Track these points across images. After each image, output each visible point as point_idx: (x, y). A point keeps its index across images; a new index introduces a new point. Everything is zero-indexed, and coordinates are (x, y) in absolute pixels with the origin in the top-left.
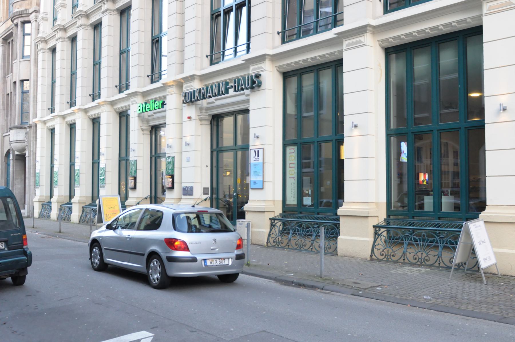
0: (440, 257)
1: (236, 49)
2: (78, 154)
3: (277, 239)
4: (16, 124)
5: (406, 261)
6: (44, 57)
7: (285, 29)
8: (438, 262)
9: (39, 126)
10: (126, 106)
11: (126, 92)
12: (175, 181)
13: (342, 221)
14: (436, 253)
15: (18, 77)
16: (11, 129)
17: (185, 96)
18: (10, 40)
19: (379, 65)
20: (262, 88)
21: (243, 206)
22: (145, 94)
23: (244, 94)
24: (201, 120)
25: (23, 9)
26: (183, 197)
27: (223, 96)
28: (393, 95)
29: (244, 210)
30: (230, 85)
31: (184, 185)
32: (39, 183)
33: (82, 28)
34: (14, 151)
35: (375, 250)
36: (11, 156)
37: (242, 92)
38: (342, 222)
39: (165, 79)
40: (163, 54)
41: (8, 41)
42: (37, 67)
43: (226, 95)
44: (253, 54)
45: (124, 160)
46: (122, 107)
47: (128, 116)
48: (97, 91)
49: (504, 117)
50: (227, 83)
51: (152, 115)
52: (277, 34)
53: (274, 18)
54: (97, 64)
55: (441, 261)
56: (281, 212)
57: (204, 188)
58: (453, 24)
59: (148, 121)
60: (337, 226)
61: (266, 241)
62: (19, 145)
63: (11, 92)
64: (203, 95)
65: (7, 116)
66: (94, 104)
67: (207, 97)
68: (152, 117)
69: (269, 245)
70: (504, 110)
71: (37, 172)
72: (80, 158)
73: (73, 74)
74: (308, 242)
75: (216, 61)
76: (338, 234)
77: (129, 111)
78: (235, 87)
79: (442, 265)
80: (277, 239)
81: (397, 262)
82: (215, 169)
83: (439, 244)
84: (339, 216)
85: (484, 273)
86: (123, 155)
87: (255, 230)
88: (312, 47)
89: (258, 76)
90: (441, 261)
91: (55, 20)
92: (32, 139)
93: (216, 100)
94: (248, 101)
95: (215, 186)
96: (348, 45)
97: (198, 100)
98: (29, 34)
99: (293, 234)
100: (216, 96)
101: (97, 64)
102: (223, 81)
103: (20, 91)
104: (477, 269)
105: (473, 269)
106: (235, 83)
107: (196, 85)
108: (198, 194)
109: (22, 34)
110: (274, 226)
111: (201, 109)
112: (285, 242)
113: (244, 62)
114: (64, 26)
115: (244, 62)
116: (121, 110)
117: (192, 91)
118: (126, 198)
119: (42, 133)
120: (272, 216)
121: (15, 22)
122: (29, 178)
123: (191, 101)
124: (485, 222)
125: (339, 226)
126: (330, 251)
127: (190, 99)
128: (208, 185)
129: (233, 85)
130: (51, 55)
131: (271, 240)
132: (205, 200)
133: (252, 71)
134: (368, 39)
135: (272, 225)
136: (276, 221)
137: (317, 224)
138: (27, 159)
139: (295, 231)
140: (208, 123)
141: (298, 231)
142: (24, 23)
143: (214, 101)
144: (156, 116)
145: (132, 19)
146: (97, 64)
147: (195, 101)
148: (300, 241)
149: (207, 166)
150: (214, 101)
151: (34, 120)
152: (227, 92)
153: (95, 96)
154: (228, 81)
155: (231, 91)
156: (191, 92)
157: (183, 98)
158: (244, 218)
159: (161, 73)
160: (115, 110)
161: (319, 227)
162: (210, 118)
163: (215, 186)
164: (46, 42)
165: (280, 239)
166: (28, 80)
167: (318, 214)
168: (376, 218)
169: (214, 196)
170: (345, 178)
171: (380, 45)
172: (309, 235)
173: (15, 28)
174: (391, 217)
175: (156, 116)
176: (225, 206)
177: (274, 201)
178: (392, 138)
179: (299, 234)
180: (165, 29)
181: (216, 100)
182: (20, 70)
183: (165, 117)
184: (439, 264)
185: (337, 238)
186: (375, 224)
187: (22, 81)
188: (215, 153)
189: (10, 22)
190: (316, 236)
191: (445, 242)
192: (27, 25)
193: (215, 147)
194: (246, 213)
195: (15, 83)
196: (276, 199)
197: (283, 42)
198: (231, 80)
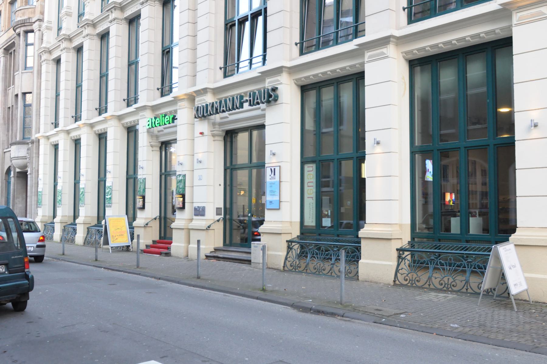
0: (467, 282)
1: (251, 60)
3: (294, 262)
4: (18, 139)
5: (432, 286)
6: (48, 69)
8: (465, 287)
9: (42, 141)
10: (134, 121)
11: (135, 106)
12: (186, 200)
14: (464, 278)
15: (20, 90)
17: (198, 110)
18: (12, 50)
20: (279, 102)
22: (154, 108)
24: (214, 136)
26: (195, 217)
27: (237, 110)
30: (245, 99)
31: (196, 205)
32: (41, 202)
33: (88, 37)
35: (399, 275)
37: (258, 106)
38: (364, 244)
39: (176, 92)
40: (174, 65)
41: (10, 52)
43: (241, 110)
44: (269, 66)
46: (130, 122)
47: (136, 131)
49: (535, 133)
50: (242, 97)
51: (162, 131)
55: (469, 287)
57: (217, 208)
60: (359, 249)
61: (282, 265)
62: (20, 162)
64: (217, 109)
67: (220, 112)
68: (161, 133)
69: (286, 268)
70: (536, 126)
71: (39, 190)
74: (327, 266)
75: (230, 74)
76: (359, 258)
77: (137, 126)
78: (250, 100)
79: (470, 290)
80: (294, 262)
81: (422, 287)
82: (228, 188)
83: (467, 269)
84: (360, 238)
85: (515, 300)
87: (270, 253)
88: (332, 58)
89: (274, 90)
90: (469, 287)
92: (34, 155)
93: (165, 128)
94: (264, 116)
95: (228, 206)
96: (369, 57)
97: (211, 114)
98: (32, 44)
100: (230, 110)
102: (237, 95)
103: (23, 105)
104: (507, 295)
105: (503, 295)
106: (250, 97)
107: (209, 99)
108: (211, 215)
109: (25, 44)
110: (291, 249)
111: (214, 124)
112: (303, 266)
113: (260, 74)
114: (69, 36)
115: (260, 74)
116: (129, 125)
117: (204, 105)
118: (134, 219)
120: (289, 238)
121: (17, 31)
122: (31, 197)
123: (203, 116)
124: (515, 245)
125: (360, 249)
127: (203, 114)
128: (222, 206)
129: (248, 98)
131: (288, 264)
132: (218, 221)
133: (268, 84)
134: (391, 50)
135: (289, 248)
136: (293, 244)
137: (337, 247)
138: (29, 176)
139: (313, 254)
141: (317, 254)
142: (26, 32)
143: (228, 116)
144: (166, 131)
145: (141, 29)
146: (104, 76)
147: (208, 115)
148: (318, 265)
149: (220, 185)
150: (228, 116)
151: (37, 135)
152: (241, 106)
153: (102, 110)
154: (242, 94)
155: (246, 105)
156: (203, 106)
157: (194, 112)
159: (171, 86)
160: (123, 124)
161: (339, 250)
162: (224, 134)
164: (50, 52)
165: (297, 263)
166: (31, 93)
168: (400, 241)
169: (228, 217)
171: (404, 57)
172: (328, 259)
174: (416, 239)
175: (166, 131)
176: (239, 227)
177: (291, 222)
178: (417, 155)
180: (176, 39)
181: (230, 115)
182: (23, 81)
183: (176, 133)
184: (467, 289)
185: (358, 262)
187: (24, 94)
188: (228, 171)
189: (11, 32)
190: (336, 260)
191: (473, 267)
192: (30, 35)
195: (17, 96)
197: (302, 53)
198: (246, 93)
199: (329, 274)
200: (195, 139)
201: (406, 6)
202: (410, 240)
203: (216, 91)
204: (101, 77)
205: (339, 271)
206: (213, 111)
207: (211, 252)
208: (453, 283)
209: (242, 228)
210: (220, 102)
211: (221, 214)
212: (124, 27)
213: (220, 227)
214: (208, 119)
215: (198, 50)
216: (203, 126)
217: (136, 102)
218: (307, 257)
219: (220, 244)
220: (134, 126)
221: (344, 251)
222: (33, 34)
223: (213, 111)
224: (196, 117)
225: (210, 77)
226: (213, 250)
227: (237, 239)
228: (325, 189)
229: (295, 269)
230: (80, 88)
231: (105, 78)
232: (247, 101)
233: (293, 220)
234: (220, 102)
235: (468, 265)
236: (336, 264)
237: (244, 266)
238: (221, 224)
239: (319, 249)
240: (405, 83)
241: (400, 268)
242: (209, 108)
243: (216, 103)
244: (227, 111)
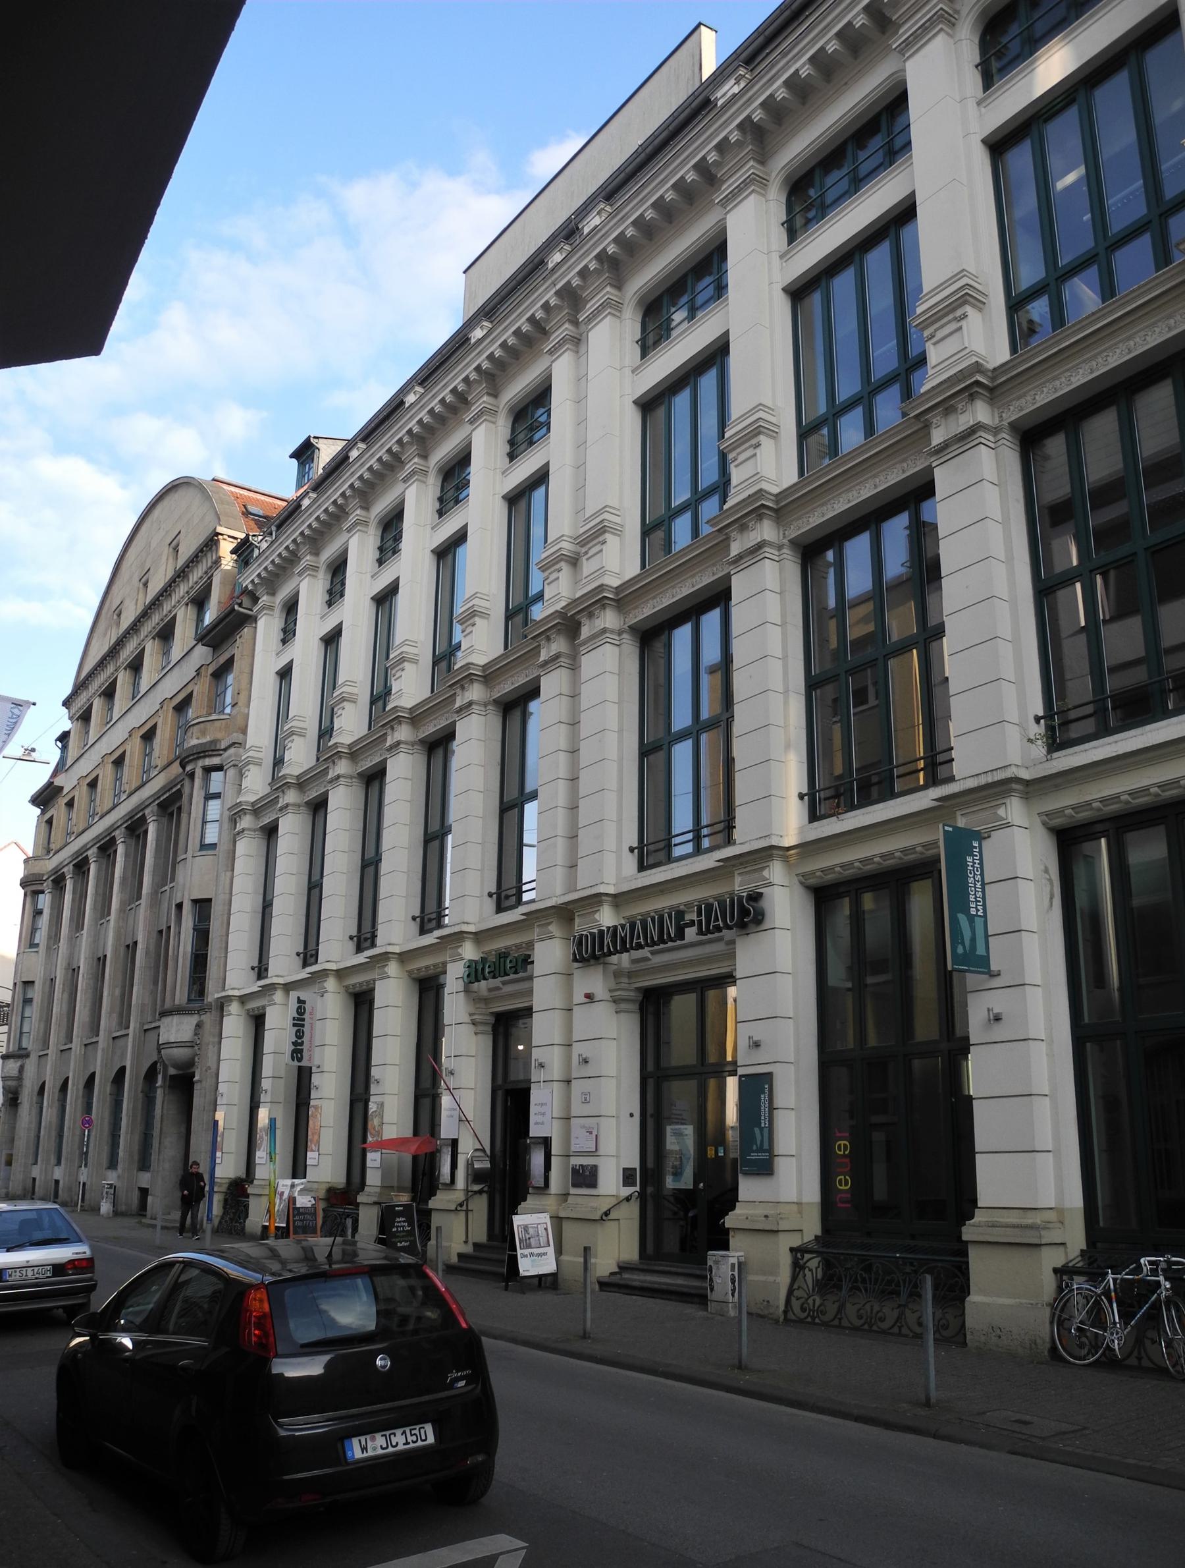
2: (266, 1084)
3: (810, 1301)
5: (1146, 1363)
6: (248, 849)
7: (1051, 708)
10: (435, 966)
11: (438, 933)
13: (973, 1254)
16: (165, 1014)
17: (580, 943)
18: (175, 808)
19: (1046, 871)
20: (766, 925)
21: (723, 1217)
23: (721, 939)
24: (615, 1001)
25: (208, 739)
26: (573, 1191)
27: (670, 944)
28: (1085, 940)
29: (727, 1226)
30: (688, 917)
31: (576, 1161)
34: (165, 1068)
35: (793, 1299)
36: (160, 1077)
37: (717, 935)
38: (978, 1262)
40: (525, 841)
41: (170, 810)
42: (233, 870)
43: (679, 942)
45: (426, 1096)
46: (427, 968)
47: (439, 988)
48: (312, 946)
50: (680, 914)
51: (498, 989)
52: (1032, 721)
53: (482, 870)
54: (315, 887)
56: (819, 1233)
57: (625, 1170)
58: (1152, 790)
59: (486, 1001)
61: (782, 1308)
62: (180, 1053)
63: (169, 928)
64: (623, 941)
65: (156, 983)
66: (430, 939)
67: (632, 948)
68: (496, 993)
69: (791, 1316)
70: (586, 1062)
72: (269, 1093)
73: (267, 906)
74: (890, 1312)
75: (651, 861)
76: (965, 1290)
77: (442, 977)
78: (700, 922)
79: (905, 1331)
80: (810, 1301)
81: (825, 1324)
82: (650, 1123)
84: (967, 1242)
86: (426, 1083)
87: (751, 1278)
88: (886, 826)
89: (755, 897)
90: (1143, 1354)
91: (278, 762)
93: (504, 983)
94: (732, 956)
95: (650, 1164)
97: (610, 954)
98: (217, 796)
99: (851, 1289)
100: (654, 944)
101: (314, 888)
102: (670, 908)
106: (699, 914)
107: (607, 918)
108: (610, 1183)
109: (203, 794)
110: (803, 1268)
111: (617, 974)
112: (831, 1309)
116: (423, 974)
117: (595, 931)
119: (234, 1025)
120: (796, 1242)
121: (188, 768)
123: (594, 957)
126: (945, 1333)
127: (591, 951)
128: (635, 1163)
129: (694, 917)
130: (265, 843)
131: (796, 1304)
132: (628, 1199)
133: (740, 885)
134: (1014, 810)
135: (798, 1267)
136: (807, 1256)
137: (912, 1264)
139: (856, 1281)
140: (635, 1007)
141: (864, 1281)
142: (208, 770)
143: (649, 955)
145: (456, 762)
146: (314, 888)
147: (605, 955)
148: (868, 1307)
149: (632, 1115)
150: (649, 955)
152: (681, 935)
154: (682, 907)
155: (691, 933)
156: (592, 934)
157: (573, 948)
158: (727, 1248)
159: (669, 840)
161: (915, 1272)
162: (492, 1020)
163: (650, 1164)
165: (818, 1302)
167: (913, 1237)
168: (1061, 1248)
169: (650, 1190)
170: (980, 1142)
171: (1044, 824)
172: (891, 1293)
173: (187, 782)
174: (1099, 1245)
176: (675, 1213)
177: (799, 1204)
178: (1088, 1045)
179: (866, 1290)
181: (504, 983)
182: (195, 877)
183: (530, 992)
185: (963, 1300)
186: (1059, 1265)
188: (651, 1082)
189: (176, 769)
190: (911, 1295)
192: (216, 776)
193: (650, 1067)
194: (731, 1234)
195: (179, 906)
196: (1067, 1205)
197: (642, 867)
198: (688, 905)
199: (896, 1330)
200: (575, 1008)
201: (1041, 714)
202: (819, 1233)
203: (619, 900)
204: (310, 889)
205: (920, 1324)
206: (615, 946)
207: (611, 1274)
208: (880, 1314)
209: (687, 1214)
210: (633, 926)
211: (634, 1184)
212: (358, 790)
213: (632, 1212)
214: (605, 964)
215: (580, 809)
216: (594, 981)
217: (373, 945)
218: (840, 1288)
219: (631, 1253)
220: (436, 977)
221: (928, 1278)
222: (221, 773)
223: (615, 946)
224: (575, 960)
225: (614, 869)
226: (617, 1270)
227: (672, 1242)
228: (875, 1119)
229: (813, 1318)
230: (317, 890)
231: (372, 868)
232: (692, 923)
233: (805, 1200)
234: (633, 926)
235: (904, 1281)
236: (910, 1306)
237: (690, 1310)
238: (634, 1209)
239: (868, 1269)
240: (1050, 880)
241: (795, 1286)
242: (607, 940)
243: (623, 926)
244: (648, 946)
